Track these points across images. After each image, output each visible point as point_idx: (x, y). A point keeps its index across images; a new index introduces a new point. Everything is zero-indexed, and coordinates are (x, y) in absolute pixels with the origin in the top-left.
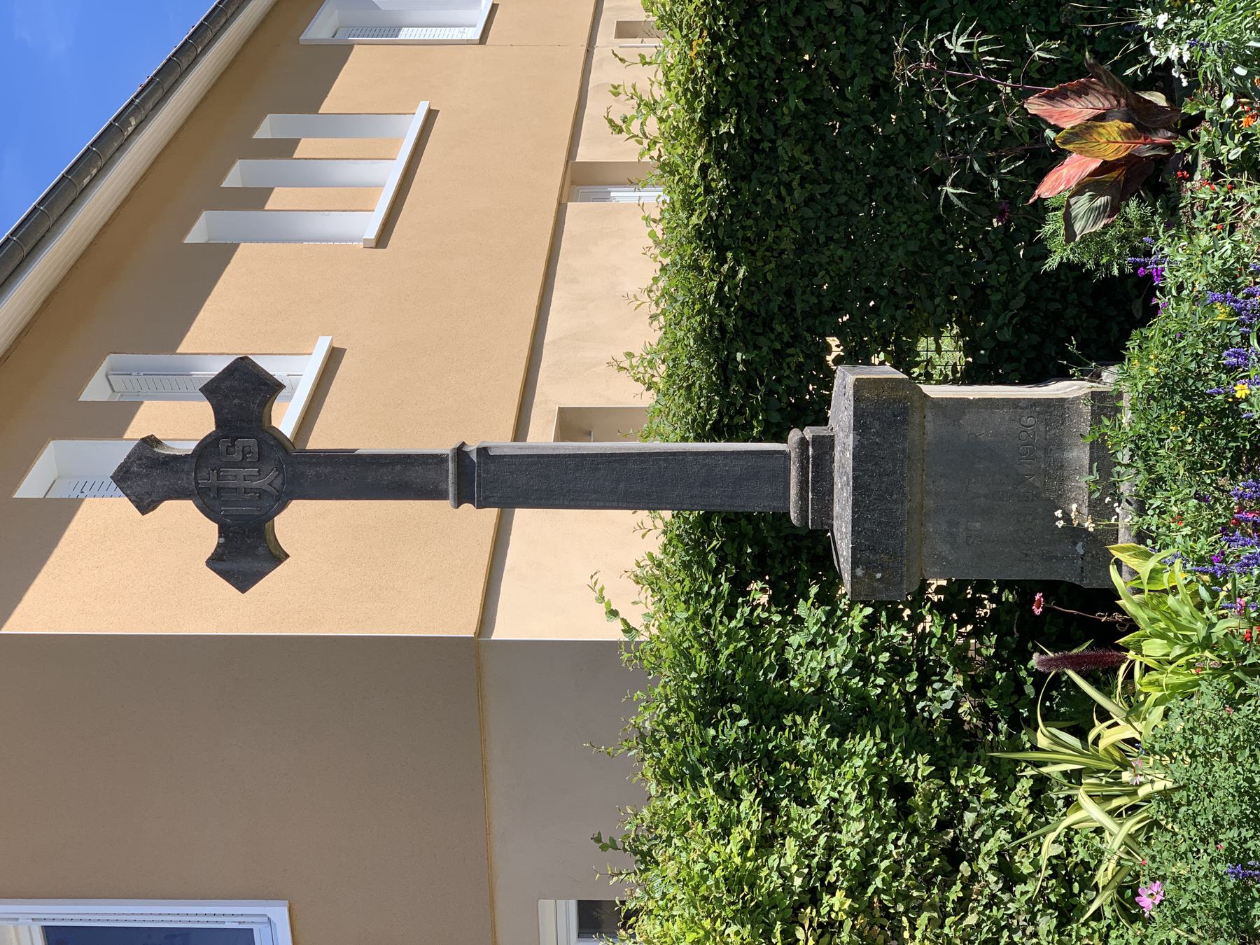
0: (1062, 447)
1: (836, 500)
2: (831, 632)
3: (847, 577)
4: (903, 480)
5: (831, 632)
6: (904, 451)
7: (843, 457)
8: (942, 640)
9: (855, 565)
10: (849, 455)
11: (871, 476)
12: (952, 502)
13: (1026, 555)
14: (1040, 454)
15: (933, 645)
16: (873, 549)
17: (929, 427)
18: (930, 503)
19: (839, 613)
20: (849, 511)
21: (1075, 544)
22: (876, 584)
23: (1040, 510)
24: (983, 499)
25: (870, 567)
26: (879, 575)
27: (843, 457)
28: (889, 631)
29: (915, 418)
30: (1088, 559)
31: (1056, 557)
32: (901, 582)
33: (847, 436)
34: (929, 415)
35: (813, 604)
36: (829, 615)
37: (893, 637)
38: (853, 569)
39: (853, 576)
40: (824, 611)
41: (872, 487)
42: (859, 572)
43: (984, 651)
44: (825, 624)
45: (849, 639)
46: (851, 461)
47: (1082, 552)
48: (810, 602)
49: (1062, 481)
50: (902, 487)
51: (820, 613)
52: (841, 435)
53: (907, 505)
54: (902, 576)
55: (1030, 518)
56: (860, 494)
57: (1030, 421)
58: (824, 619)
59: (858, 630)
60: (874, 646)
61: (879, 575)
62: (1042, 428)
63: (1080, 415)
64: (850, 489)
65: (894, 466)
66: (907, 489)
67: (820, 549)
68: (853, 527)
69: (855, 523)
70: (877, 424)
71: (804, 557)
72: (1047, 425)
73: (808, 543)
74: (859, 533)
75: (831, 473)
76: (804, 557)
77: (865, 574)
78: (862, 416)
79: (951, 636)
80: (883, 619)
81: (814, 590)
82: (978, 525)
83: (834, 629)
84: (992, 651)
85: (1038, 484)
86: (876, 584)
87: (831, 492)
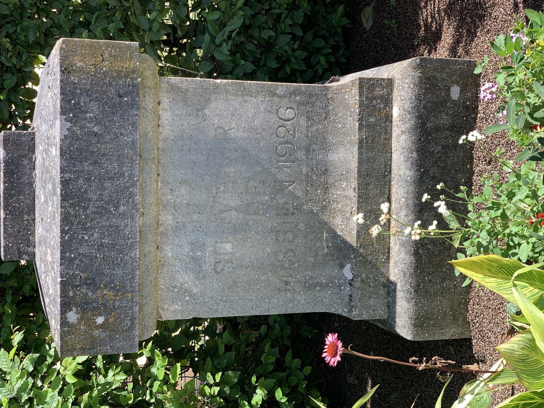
0: (325, 147)
1: (38, 219)
2: (39, 383)
3: (54, 324)
4: (133, 185)
5: (39, 383)
6: (133, 143)
7: (48, 160)
8: (166, 381)
9: (65, 307)
10: (55, 152)
11: (88, 180)
12: (195, 217)
13: (287, 283)
14: (301, 155)
15: (155, 389)
16: (91, 283)
17: (166, 116)
18: (168, 219)
19: (49, 360)
20: (57, 231)
21: (342, 266)
22: (96, 333)
23: (302, 226)
24: (234, 214)
25: (87, 308)
26: (100, 320)
27: (48, 160)
28: (105, 376)
29: (148, 102)
30: (358, 284)
31: (320, 285)
32: (132, 328)
33: (52, 126)
34: (165, 101)
35: (17, 354)
36: (38, 363)
37: (110, 384)
38: (63, 312)
39: (64, 323)
40: (32, 360)
41: (90, 195)
42: (73, 317)
43: (207, 389)
44: (32, 375)
45: (60, 393)
46: (58, 160)
47: (350, 276)
48: (13, 351)
49: (326, 189)
50: (131, 195)
51: (28, 364)
52: (44, 127)
53: (140, 221)
54: (133, 319)
55: (290, 236)
56: (73, 205)
57: (289, 113)
58: (31, 369)
59: (71, 380)
60: (90, 397)
61: (100, 320)
62: (303, 122)
63: (347, 107)
64: (57, 199)
65: (121, 166)
66: (138, 199)
67: (27, 289)
68: (63, 252)
69: (65, 247)
70: (94, 106)
71: (9, 299)
72: (309, 118)
73: (13, 283)
74: (71, 261)
75: (31, 184)
76: (9, 299)
77: (80, 320)
78: (73, 94)
79: (174, 377)
80: (99, 364)
81: (17, 338)
82: (228, 247)
83: (43, 379)
84: (216, 389)
85: (300, 194)
86: (96, 333)
87: (32, 210)
